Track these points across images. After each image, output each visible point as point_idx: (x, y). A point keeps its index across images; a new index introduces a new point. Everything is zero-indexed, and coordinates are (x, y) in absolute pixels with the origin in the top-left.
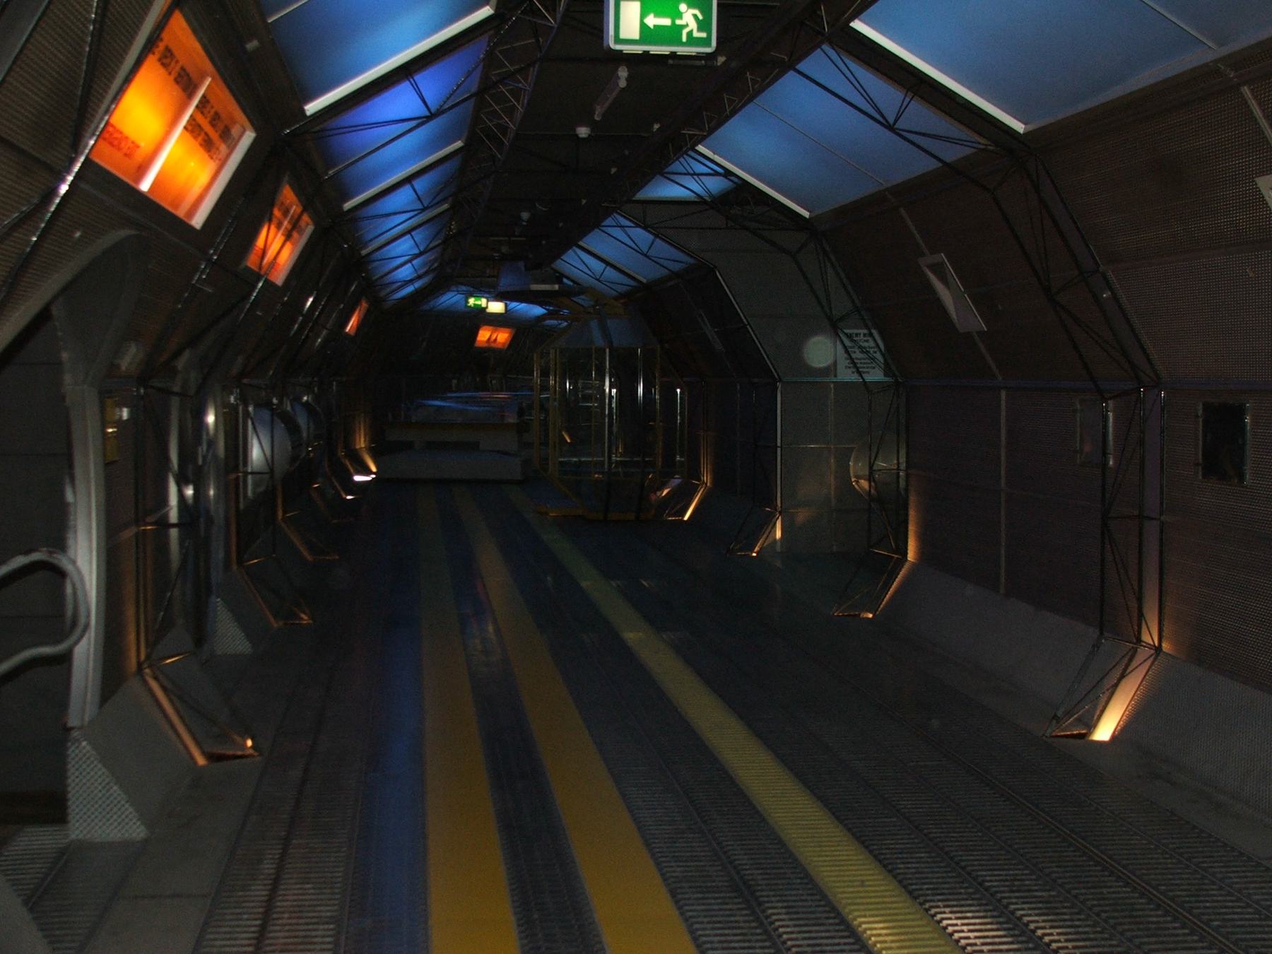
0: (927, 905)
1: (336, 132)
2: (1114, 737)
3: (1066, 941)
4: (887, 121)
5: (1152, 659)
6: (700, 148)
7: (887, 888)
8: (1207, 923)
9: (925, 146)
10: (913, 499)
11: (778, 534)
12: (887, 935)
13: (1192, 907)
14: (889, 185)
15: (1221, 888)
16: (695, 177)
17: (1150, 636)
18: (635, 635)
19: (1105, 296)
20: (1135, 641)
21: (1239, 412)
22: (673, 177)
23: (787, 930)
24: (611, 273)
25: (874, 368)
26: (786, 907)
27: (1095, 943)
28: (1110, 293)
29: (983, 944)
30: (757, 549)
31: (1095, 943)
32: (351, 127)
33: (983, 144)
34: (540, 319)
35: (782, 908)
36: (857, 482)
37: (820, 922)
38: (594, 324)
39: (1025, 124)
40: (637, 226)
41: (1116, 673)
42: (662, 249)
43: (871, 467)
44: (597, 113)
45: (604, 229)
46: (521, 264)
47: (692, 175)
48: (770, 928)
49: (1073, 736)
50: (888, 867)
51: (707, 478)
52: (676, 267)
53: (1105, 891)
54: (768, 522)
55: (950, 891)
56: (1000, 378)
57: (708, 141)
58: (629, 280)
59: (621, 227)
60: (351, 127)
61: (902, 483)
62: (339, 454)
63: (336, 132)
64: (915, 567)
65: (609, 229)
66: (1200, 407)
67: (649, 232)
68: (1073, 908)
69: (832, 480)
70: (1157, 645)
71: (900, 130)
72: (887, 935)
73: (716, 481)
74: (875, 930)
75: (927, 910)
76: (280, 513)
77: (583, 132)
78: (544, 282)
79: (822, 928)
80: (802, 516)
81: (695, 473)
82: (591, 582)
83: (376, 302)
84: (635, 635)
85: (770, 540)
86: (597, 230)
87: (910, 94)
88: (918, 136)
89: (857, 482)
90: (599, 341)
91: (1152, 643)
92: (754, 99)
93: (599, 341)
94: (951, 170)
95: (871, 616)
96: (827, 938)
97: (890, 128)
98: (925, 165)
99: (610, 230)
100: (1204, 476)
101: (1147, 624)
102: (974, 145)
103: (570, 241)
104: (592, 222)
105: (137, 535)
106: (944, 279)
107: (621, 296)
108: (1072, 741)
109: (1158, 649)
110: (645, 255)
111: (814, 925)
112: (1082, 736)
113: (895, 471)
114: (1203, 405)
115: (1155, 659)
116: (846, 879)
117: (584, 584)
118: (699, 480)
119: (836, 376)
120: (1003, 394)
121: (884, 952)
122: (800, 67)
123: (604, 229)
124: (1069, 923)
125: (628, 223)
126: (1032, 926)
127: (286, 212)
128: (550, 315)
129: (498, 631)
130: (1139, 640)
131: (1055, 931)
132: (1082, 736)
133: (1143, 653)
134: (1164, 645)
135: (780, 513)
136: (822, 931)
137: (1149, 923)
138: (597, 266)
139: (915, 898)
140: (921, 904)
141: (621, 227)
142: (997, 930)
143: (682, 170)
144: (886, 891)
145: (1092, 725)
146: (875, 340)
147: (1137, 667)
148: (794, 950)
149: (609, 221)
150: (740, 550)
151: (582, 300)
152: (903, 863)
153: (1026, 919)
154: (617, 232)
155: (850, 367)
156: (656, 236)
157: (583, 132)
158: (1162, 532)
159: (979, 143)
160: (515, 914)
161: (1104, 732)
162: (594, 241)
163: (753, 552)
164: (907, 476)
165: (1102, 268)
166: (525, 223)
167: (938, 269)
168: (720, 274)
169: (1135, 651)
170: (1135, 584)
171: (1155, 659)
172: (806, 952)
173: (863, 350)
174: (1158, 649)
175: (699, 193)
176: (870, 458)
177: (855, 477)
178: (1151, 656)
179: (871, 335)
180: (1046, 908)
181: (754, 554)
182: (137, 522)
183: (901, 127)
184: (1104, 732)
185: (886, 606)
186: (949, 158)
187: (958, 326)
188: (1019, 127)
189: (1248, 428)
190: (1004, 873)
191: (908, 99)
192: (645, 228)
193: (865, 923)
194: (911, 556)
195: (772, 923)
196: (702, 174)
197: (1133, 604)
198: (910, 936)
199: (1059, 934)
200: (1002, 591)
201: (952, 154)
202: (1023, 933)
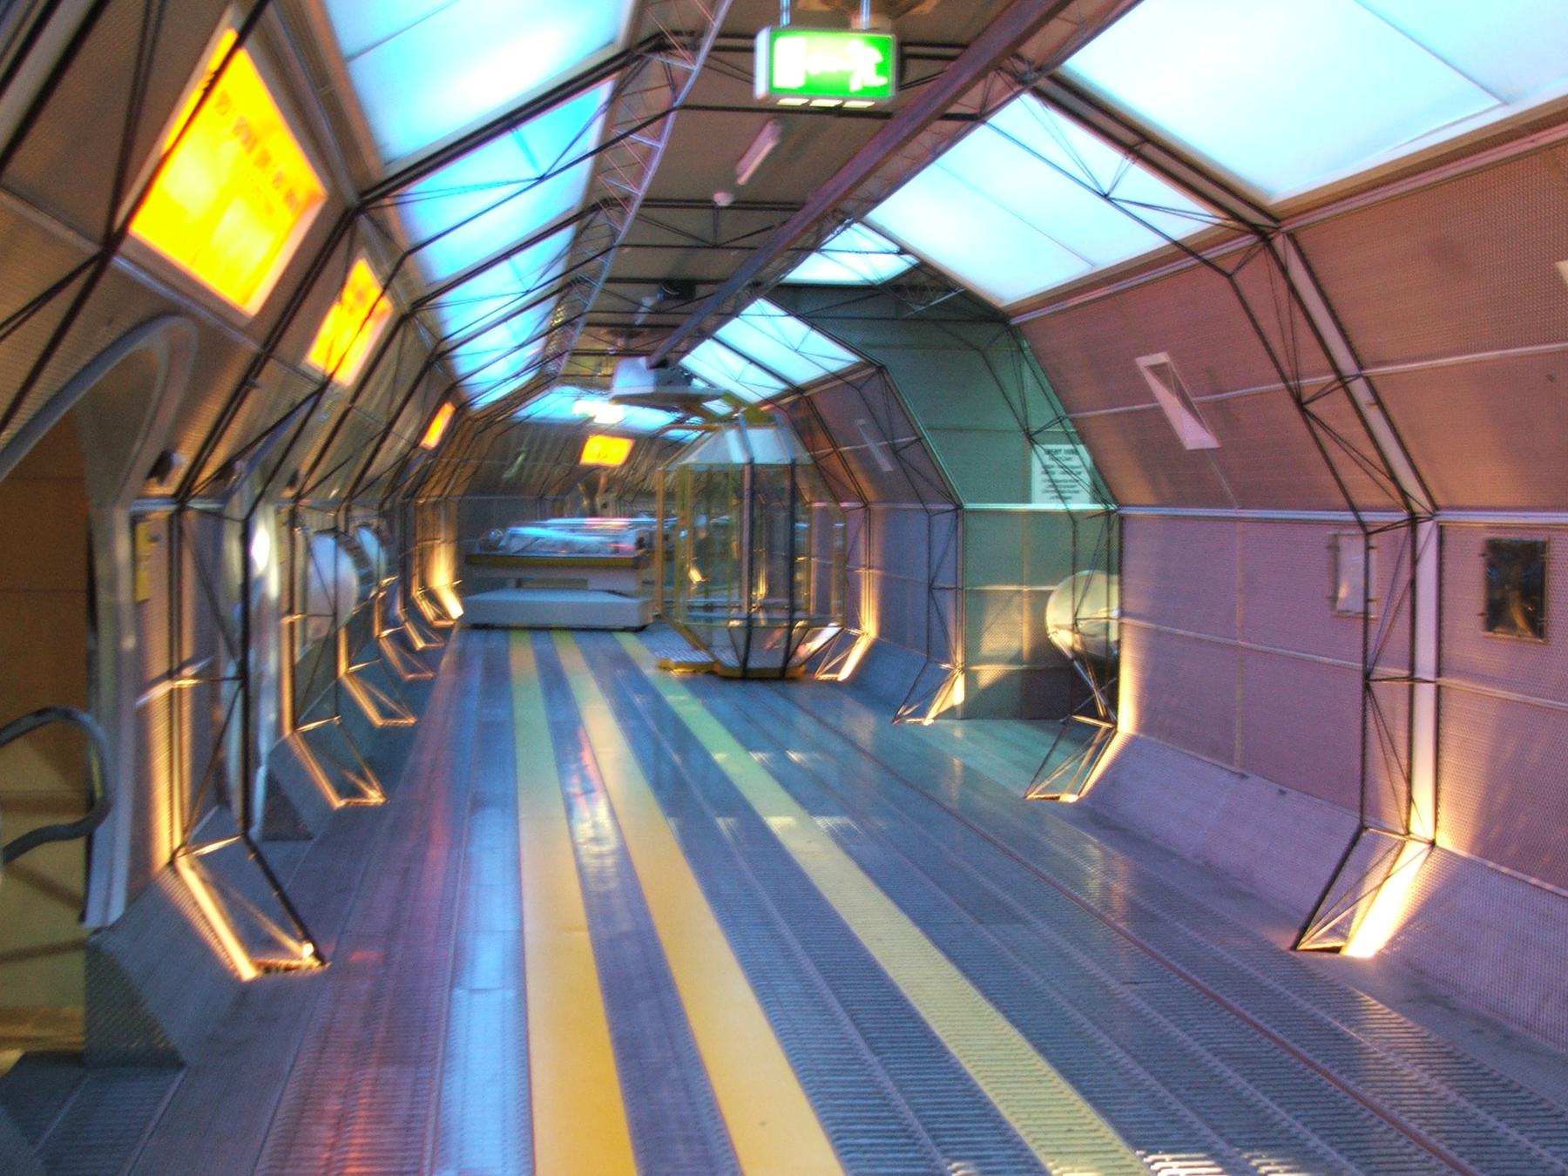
1: (426, 196)
20: (1402, 832)
25: (1077, 492)
32: (375, 188)
43: (1075, 615)
46: (642, 361)
60: (375, 188)
61: (1114, 636)
62: (413, 593)
63: (426, 196)
64: (1132, 744)
69: (1025, 630)
71: (550, 170)
76: (343, 667)
83: (462, 408)
86: (856, 226)
94: (1182, 249)
98: (1150, 243)
105: (171, 691)
108: (1326, 956)
112: (1336, 950)
113: (1105, 621)
117: (719, 757)
122: (722, 333)
127: (360, 296)
128: (679, 423)
129: (613, 813)
146: (1081, 459)
150: (910, 716)
155: (1047, 492)
164: (1121, 625)
170: (1404, 762)
171: (1429, 856)
173: (1067, 470)
179: (1076, 452)
182: (171, 674)
197: (1402, 788)
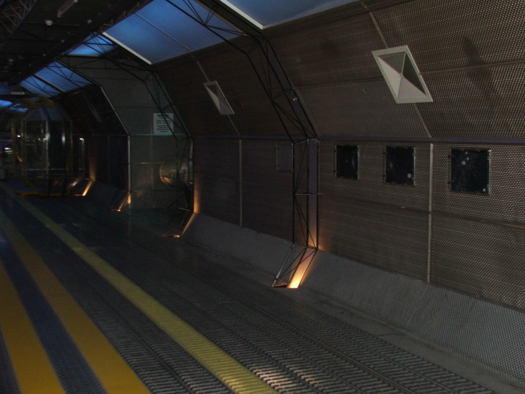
0: (251, 369)
2: (299, 286)
3: (315, 380)
4: (202, 21)
5: (314, 252)
6: (105, 34)
7: (231, 362)
8: (368, 366)
9: (217, 33)
10: (196, 186)
11: (129, 201)
12: (239, 384)
13: (318, 351)
14: (193, 50)
15: (367, 351)
16: (100, 46)
17: (312, 243)
18: (79, 249)
19: (294, 100)
21: (355, 148)
22: (89, 45)
23: (194, 386)
24: (48, 88)
26: (190, 375)
27: (327, 380)
28: (296, 99)
29: (281, 385)
30: (120, 208)
31: (327, 380)
33: (241, 33)
34: (9, 106)
35: (188, 375)
36: (163, 179)
37: (207, 380)
38: (41, 110)
39: (263, 25)
40: (65, 67)
41: (298, 260)
42: (76, 77)
44: (59, 14)
45: (50, 68)
47: (98, 44)
48: (186, 386)
49: (281, 287)
50: (228, 352)
51: (93, 177)
52: (82, 85)
53: (322, 356)
54: (125, 197)
55: (259, 361)
56: (239, 135)
57: (109, 30)
58: (55, 90)
59: (58, 67)
64: (198, 216)
65: (52, 68)
66: (336, 147)
67: (71, 70)
68: (374, 378)
70: (316, 246)
72: (239, 384)
73: (98, 178)
74: (232, 382)
75: (252, 371)
77: (49, 23)
78: (17, 91)
79: (209, 384)
80: (139, 193)
81: (88, 175)
82: (50, 224)
84: (79, 249)
85: (126, 204)
87: (212, 12)
88: (218, 30)
89: (163, 179)
90: (44, 117)
91: (314, 246)
92: (136, 12)
93: (44, 117)
95: (178, 236)
96: (213, 388)
97: (205, 25)
99: (52, 68)
100: (337, 176)
101: (311, 237)
102: (237, 33)
103: (31, 72)
104: (44, 64)
106: (216, 93)
107: (53, 98)
109: (317, 249)
110: (69, 80)
111: (204, 382)
114: (337, 146)
115: (316, 253)
116: (211, 359)
118: (89, 178)
119: (153, 134)
120: (240, 141)
121: (240, 393)
123: (50, 68)
124: (313, 372)
125: (61, 66)
126: (299, 375)
130: (307, 245)
131: (309, 376)
132: (285, 286)
133: (309, 251)
134: (319, 247)
135: (131, 192)
136: (209, 385)
137: (345, 369)
138: (42, 85)
139: (245, 365)
140: (248, 368)
141: (58, 67)
142: (281, 375)
143: (93, 42)
144: (230, 363)
145: (289, 282)
147: (307, 258)
148: (197, 392)
149: (52, 65)
151: (33, 100)
152: (233, 349)
153: (295, 372)
154: (55, 69)
156: (74, 72)
157: (49, 23)
158: (318, 200)
159: (239, 32)
160: (65, 389)
161: (295, 284)
162: (44, 74)
163: (118, 209)
165: (293, 88)
166: (11, 64)
167: (214, 89)
168: (104, 90)
169: (306, 250)
171: (316, 253)
172: (202, 393)
174: (317, 249)
175: (101, 52)
176: (177, 168)
177: (162, 176)
178: (314, 251)
180: (302, 366)
181: (119, 210)
183: (209, 25)
184: (295, 284)
185: (186, 231)
186: (228, 39)
187: (220, 112)
188: (261, 26)
189: (359, 156)
190: (278, 351)
191: (211, 14)
192: (69, 68)
193: (228, 379)
194: (196, 210)
195: (186, 383)
196: (103, 44)
198: (250, 384)
199: (311, 377)
200: (241, 225)
201: (229, 37)
202: (296, 379)
